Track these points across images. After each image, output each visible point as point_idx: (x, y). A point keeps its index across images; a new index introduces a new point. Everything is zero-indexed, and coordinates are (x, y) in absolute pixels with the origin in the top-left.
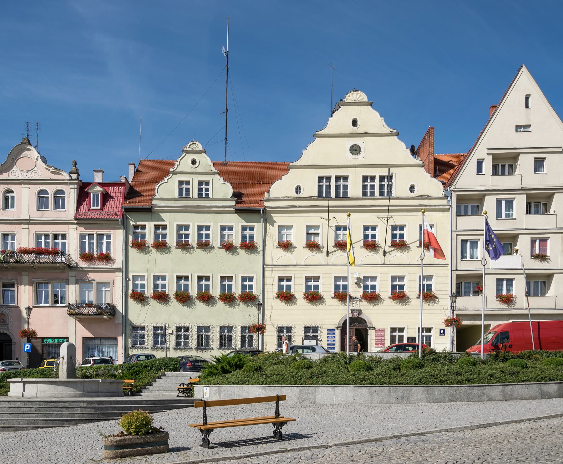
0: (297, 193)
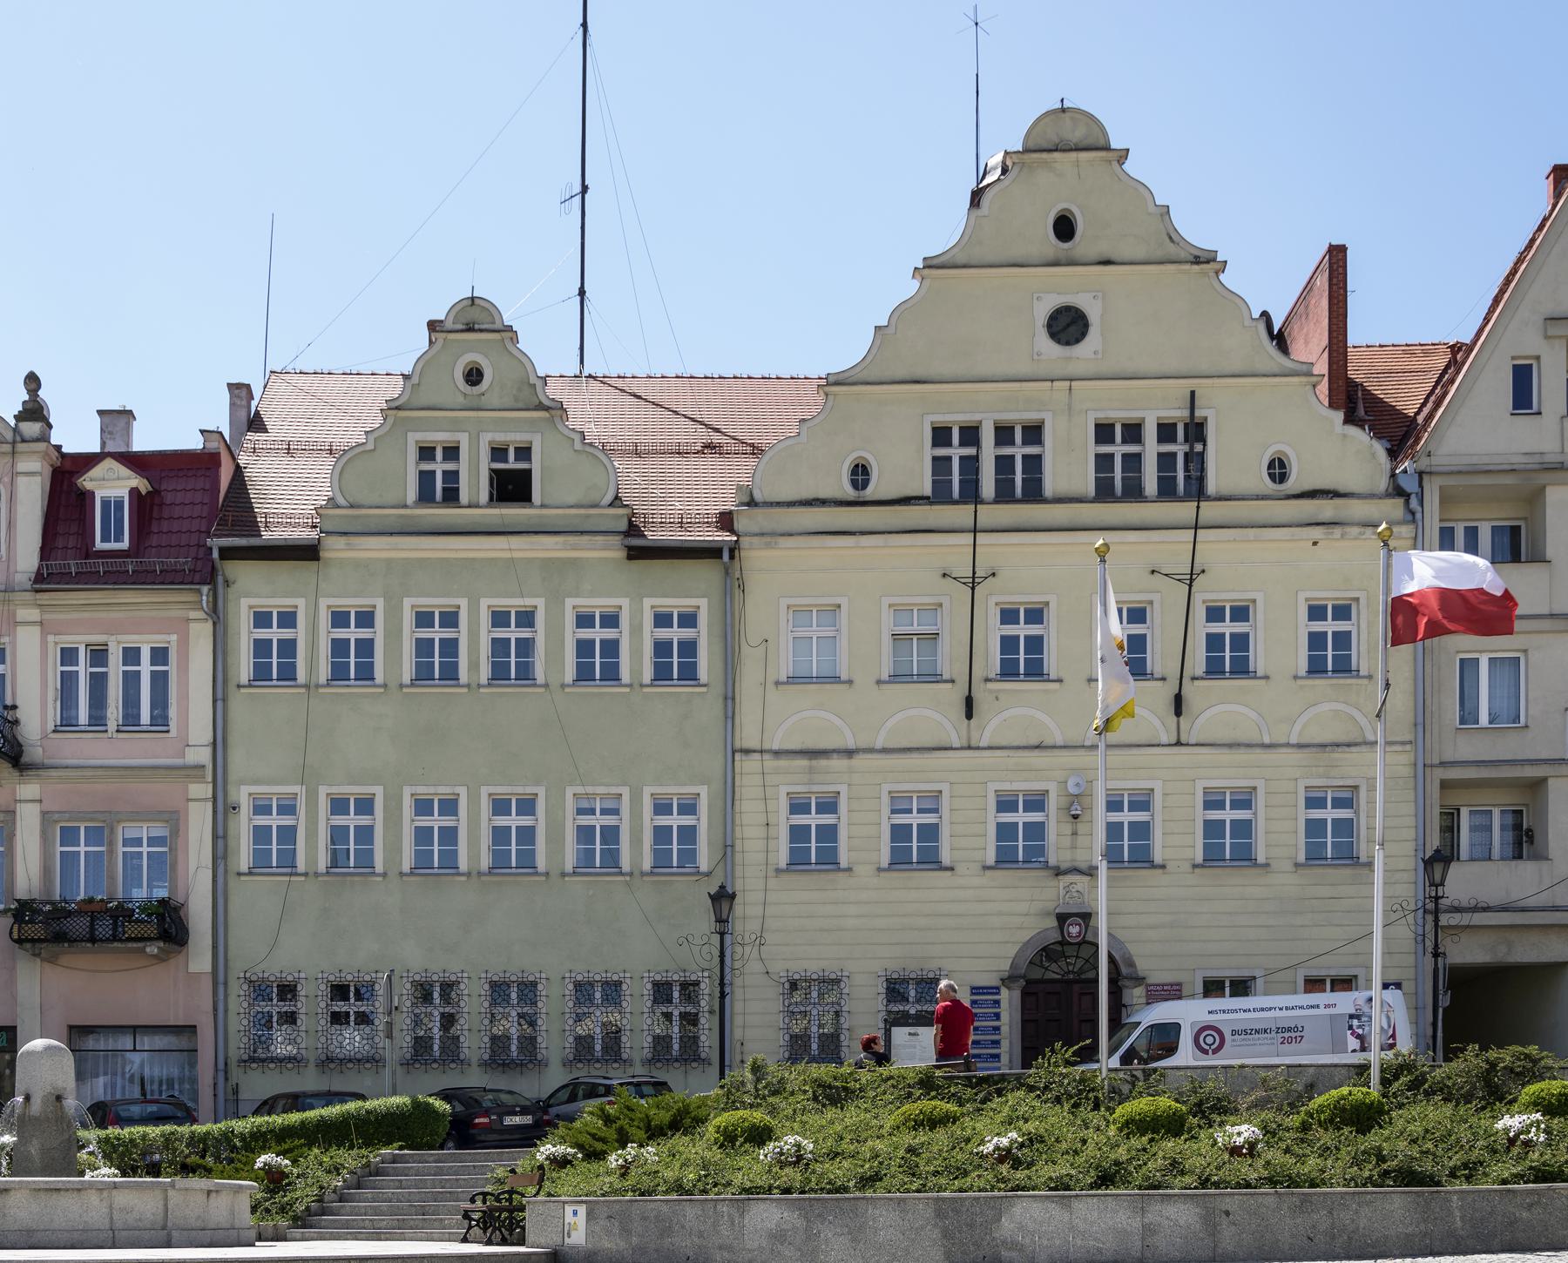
0: (855, 484)
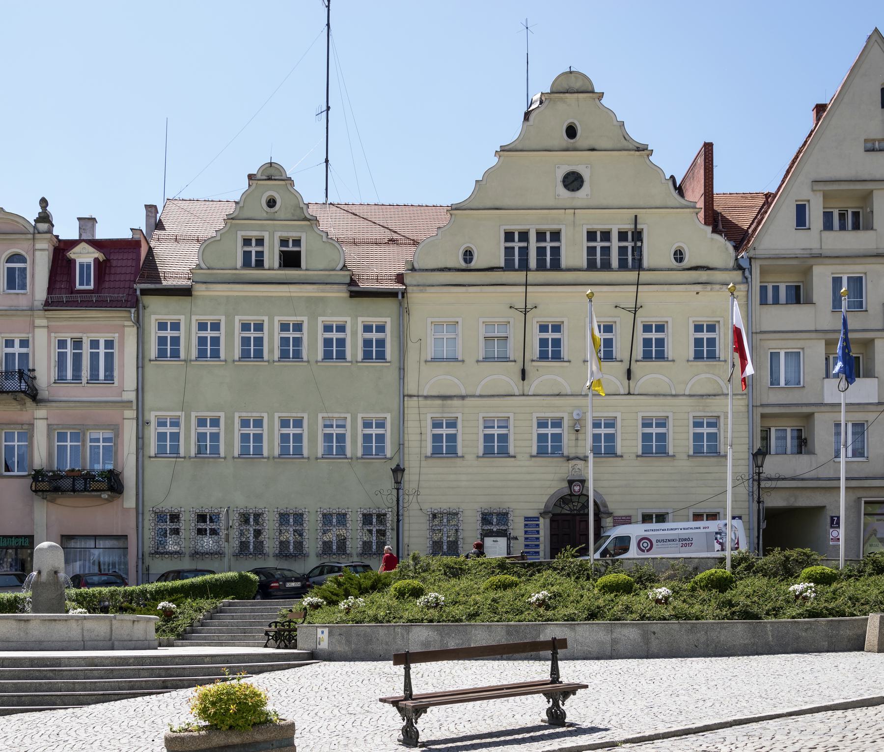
0: (465, 260)
